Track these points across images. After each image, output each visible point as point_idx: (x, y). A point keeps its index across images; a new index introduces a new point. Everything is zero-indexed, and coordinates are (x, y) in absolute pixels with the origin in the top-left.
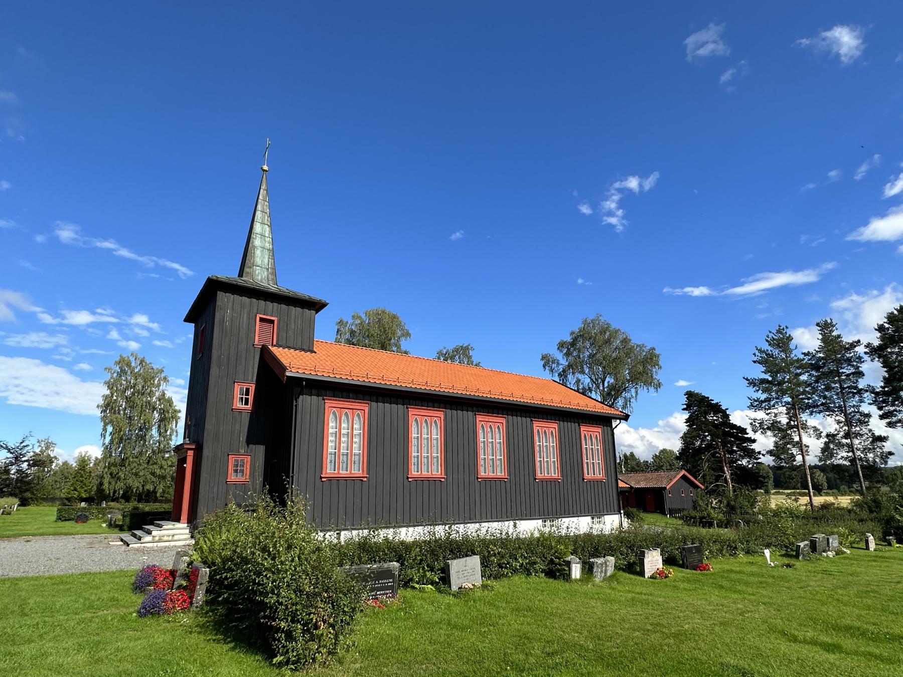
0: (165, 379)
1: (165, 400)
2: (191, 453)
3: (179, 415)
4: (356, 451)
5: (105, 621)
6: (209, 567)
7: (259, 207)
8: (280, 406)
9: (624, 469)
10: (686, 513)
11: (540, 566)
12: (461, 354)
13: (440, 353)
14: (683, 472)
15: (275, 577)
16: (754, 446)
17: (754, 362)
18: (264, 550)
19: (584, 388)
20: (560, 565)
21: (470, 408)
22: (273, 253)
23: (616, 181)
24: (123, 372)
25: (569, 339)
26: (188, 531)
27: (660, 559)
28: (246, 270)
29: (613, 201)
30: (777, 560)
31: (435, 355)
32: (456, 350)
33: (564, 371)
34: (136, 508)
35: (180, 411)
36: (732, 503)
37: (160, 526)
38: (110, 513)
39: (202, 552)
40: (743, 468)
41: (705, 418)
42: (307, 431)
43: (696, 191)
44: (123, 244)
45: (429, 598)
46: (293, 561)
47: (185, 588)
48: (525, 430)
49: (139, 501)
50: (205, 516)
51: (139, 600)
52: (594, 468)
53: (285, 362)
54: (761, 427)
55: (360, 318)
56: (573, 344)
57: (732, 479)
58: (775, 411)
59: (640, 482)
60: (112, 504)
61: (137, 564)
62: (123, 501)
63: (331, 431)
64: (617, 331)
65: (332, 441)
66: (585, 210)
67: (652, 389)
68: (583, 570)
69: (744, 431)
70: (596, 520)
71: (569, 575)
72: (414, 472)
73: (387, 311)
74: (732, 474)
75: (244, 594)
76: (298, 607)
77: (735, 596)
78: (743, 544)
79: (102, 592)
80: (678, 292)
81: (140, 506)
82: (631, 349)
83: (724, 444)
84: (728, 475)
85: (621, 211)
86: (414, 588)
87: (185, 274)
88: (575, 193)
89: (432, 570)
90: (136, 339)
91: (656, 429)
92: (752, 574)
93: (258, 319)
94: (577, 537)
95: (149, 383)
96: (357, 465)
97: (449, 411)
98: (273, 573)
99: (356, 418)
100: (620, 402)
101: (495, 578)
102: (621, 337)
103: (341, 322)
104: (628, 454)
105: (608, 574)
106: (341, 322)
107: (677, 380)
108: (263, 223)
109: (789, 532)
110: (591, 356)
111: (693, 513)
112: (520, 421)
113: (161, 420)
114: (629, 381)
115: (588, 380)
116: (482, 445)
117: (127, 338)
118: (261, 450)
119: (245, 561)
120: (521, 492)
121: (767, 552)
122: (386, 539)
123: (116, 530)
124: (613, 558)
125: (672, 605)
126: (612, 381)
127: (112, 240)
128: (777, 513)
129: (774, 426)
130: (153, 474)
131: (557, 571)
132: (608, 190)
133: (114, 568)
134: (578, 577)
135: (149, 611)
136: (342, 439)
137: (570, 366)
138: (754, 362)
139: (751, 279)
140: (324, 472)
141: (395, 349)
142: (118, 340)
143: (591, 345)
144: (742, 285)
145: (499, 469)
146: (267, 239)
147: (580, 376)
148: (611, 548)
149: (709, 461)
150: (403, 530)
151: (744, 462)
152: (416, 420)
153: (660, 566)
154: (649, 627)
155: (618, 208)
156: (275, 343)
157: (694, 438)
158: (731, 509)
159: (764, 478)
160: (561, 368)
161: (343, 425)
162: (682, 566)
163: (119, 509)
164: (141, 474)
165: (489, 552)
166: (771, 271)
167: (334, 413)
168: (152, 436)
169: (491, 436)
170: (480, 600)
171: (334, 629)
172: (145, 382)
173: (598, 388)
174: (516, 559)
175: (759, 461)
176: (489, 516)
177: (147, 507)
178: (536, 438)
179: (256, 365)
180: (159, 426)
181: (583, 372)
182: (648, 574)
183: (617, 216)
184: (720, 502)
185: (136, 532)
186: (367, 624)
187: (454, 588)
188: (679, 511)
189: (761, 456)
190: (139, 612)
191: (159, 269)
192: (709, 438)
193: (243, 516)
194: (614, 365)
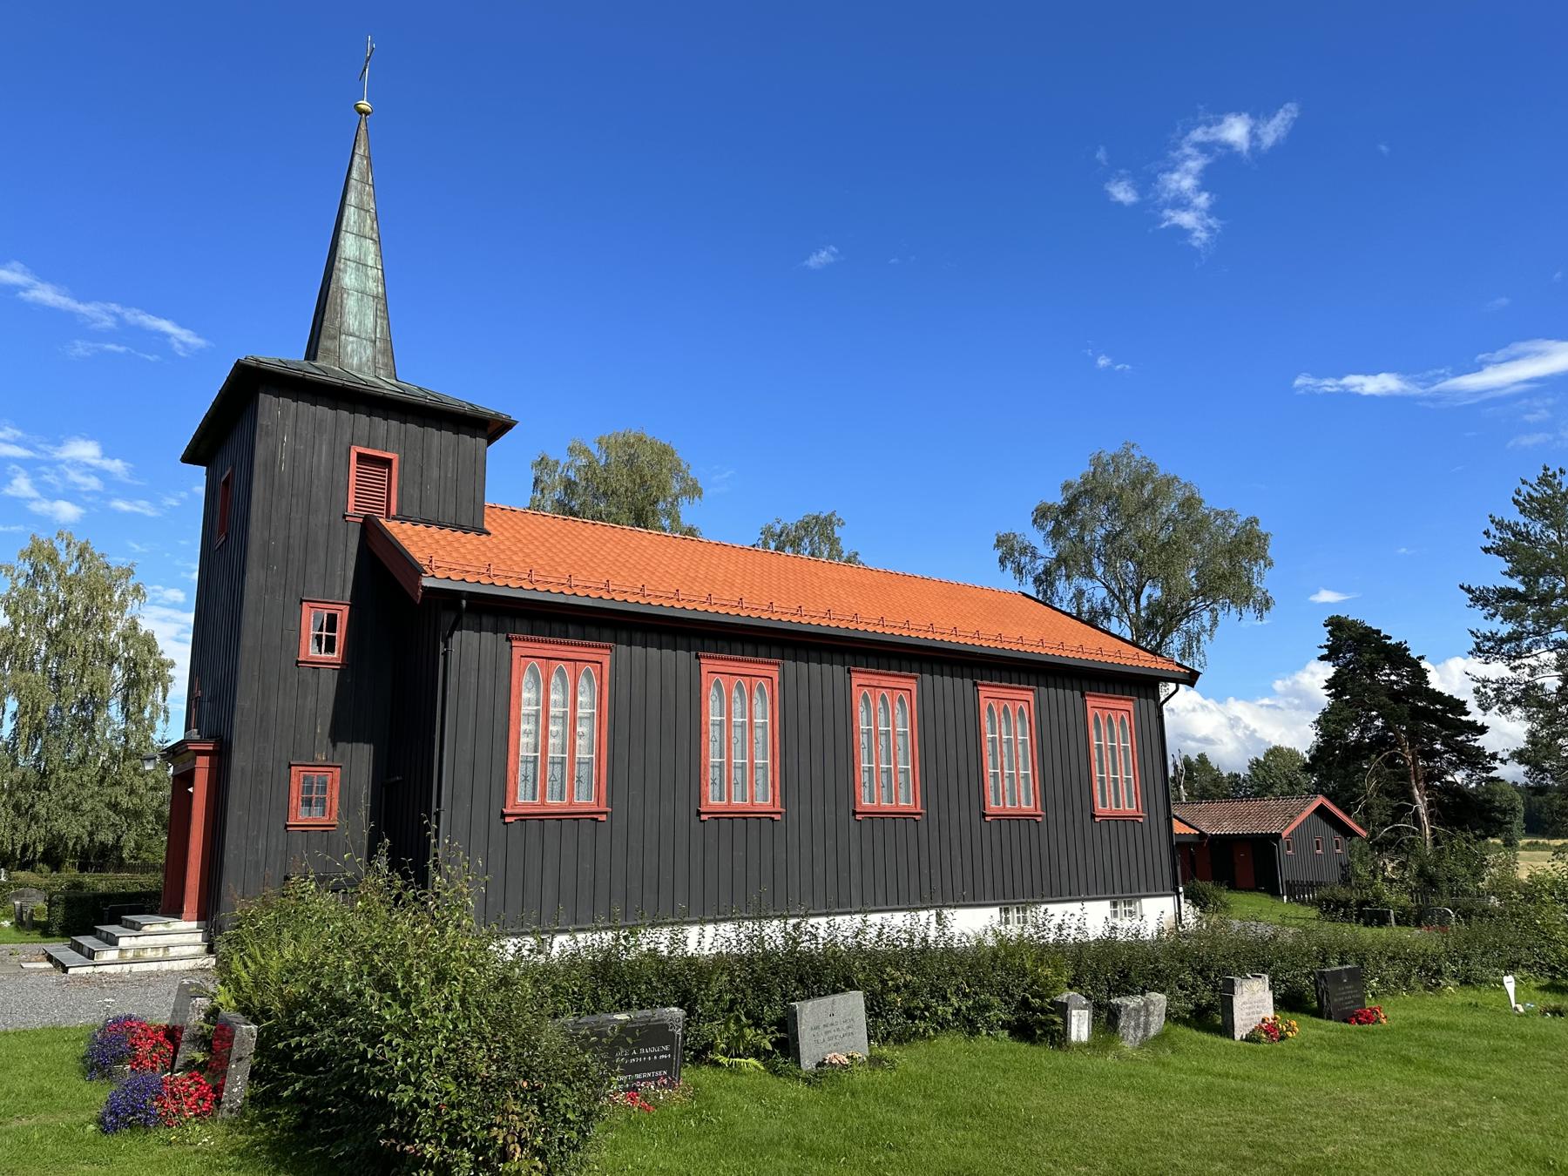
0: (137, 589)
1: (138, 639)
2: (203, 763)
3: (171, 672)
4: (582, 754)
5: (26, 1142)
6: (256, 1021)
7: (352, 198)
8: (406, 653)
9: (1184, 793)
10: (1325, 892)
11: (999, 1013)
12: (812, 536)
13: (768, 533)
14: (1320, 800)
15: (410, 1045)
16: (1482, 741)
17: (1486, 550)
18: (383, 984)
19: (1092, 610)
20: (1043, 1011)
21: (837, 658)
22: (384, 301)
23: (1198, 125)
24: (38, 575)
25: (1058, 499)
26: (199, 938)
27: (1268, 998)
28: (325, 343)
29: (1188, 172)
30: (1530, 998)
31: (755, 537)
32: (805, 526)
33: (1047, 572)
34: (77, 886)
35: (172, 664)
36: (1431, 869)
37: (136, 927)
38: (17, 896)
39: (239, 988)
40: (1455, 790)
41: (1372, 677)
42: (472, 710)
43: (1383, 148)
44: (45, 275)
45: (751, 1087)
46: (448, 1008)
47: (202, 1067)
48: (1062, 713)
49: (83, 868)
50: (236, 904)
51: (99, 1094)
52: (1117, 788)
53: (418, 554)
54: (1499, 697)
55: (586, 452)
56: (1069, 510)
57: (1431, 816)
58: (1532, 661)
59: (1219, 821)
60: (22, 875)
61: (90, 1014)
62: (46, 868)
63: (525, 709)
64: (1170, 482)
65: (527, 733)
66: (1123, 193)
67: (1249, 614)
68: (1095, 1021)
69: (1460, 707)
70: (1121, 908)
71: (1065, 1033)
72: (713, 800)
73: (648, 437)
74: (1430, 805)
75: (340, 1082)
76: (464, 1112)
77: (1438, 1081)
78: (1455, 963)
79: (14, 1078)
80: (1329, 385)
81: (88, 878)
82: (1204, 522)
83: (1413, 736)
84: (1421, 805)
85: (1205, 196)
86: (717, 1064)
87: (185, 344)
88: (1101, 155)
89: (757, 1025)
90: (72, 495)
91: (1266, 701)
92: (1476, 1032)
93: (354, 457)
94: (1081, 946)
95: (100, 601)
96: (583, 788)
97: (790, 664)
98: (407, 1036)
99: (583, 681)
100: (1176, 642)
101: (898, 1041)
102: (1179, 494)
103: (542, 463)
104: (1194, 758)
105: (1152, 1032)
106: (542, 463)
107: (1313, 590)
108: (361, 236)
109: (1559, 935)
110: (1111, 538)
111: (1342, 893)
112: (946, 684)
113: (132, 684)
114: (1196, 594)
115: (1101, 593)
116: (864, 739)
117: (50, 493)
118: (362, 755)
119: (343, 1009)
120: (953, 846)
121: (1509, 982)
122: (653, 952)
123: (35, 935)
124: (1162, 997)
125: (1297, 1101)
126: (1158, 594)
127: (15, 264)
128: (1532, 892)
129: (1529, 697)
130: (114, 806)
131: (1036, 1025)
132: (1177, 147)
133: (36, 1022)
134: (1084, 1037)
135: (123, 1118)
136: (551, 725)
137: (1061, 560)
138: (1486, 550)
139: (1500, 355)
140: (510, 802)
141: (666, 522)
142: (33, 500)
143: (1110, 513)
144: (1478, 368)
145: (902, 793)
146: (372, 273)
147: (1086, 584)
148: (1157, 974)
149: (1377, 774)
150: (693, 932)
151: (1459, 777)
152: (717, 684)
153: (1269, 1012)
154: (1246, 1152)
155: (1199, 189)
156: (393, 511)
157: (1346, 722)
158: (1428, 882)
159: (1504, 812)
160: (1040, 565)
161: (553, 697)
162: (1318, 1013)
163: (38, 888)
164: (86, 806)
165: (884, 982)
166: (1549, 338)
167: (533, 671)
168: (108, 720)
169: (1008, 727)
170: (866, 1091)
171: (543, 1160)
172: (92, 598)
173: (1126, 609)
174: (945, 998)
175: (1493, 774)
176: (880, 898)
177: (100, 882)
178: (1093, 733)
179: (352, 564)
180: (126, 698)
181: (1090, 575)
182: (1240, 1032)
183: (1196, 209)
184: (1403, 865)
185: (81, 940)
186: (616, 1146)
187: (808, 1064)
188: (1311, 886)
189: (1497, 764)
190: (100, 1121)
191: (128, 333)
192: (1379, 723)
193: (327, 903)
194: (1166, 563)
